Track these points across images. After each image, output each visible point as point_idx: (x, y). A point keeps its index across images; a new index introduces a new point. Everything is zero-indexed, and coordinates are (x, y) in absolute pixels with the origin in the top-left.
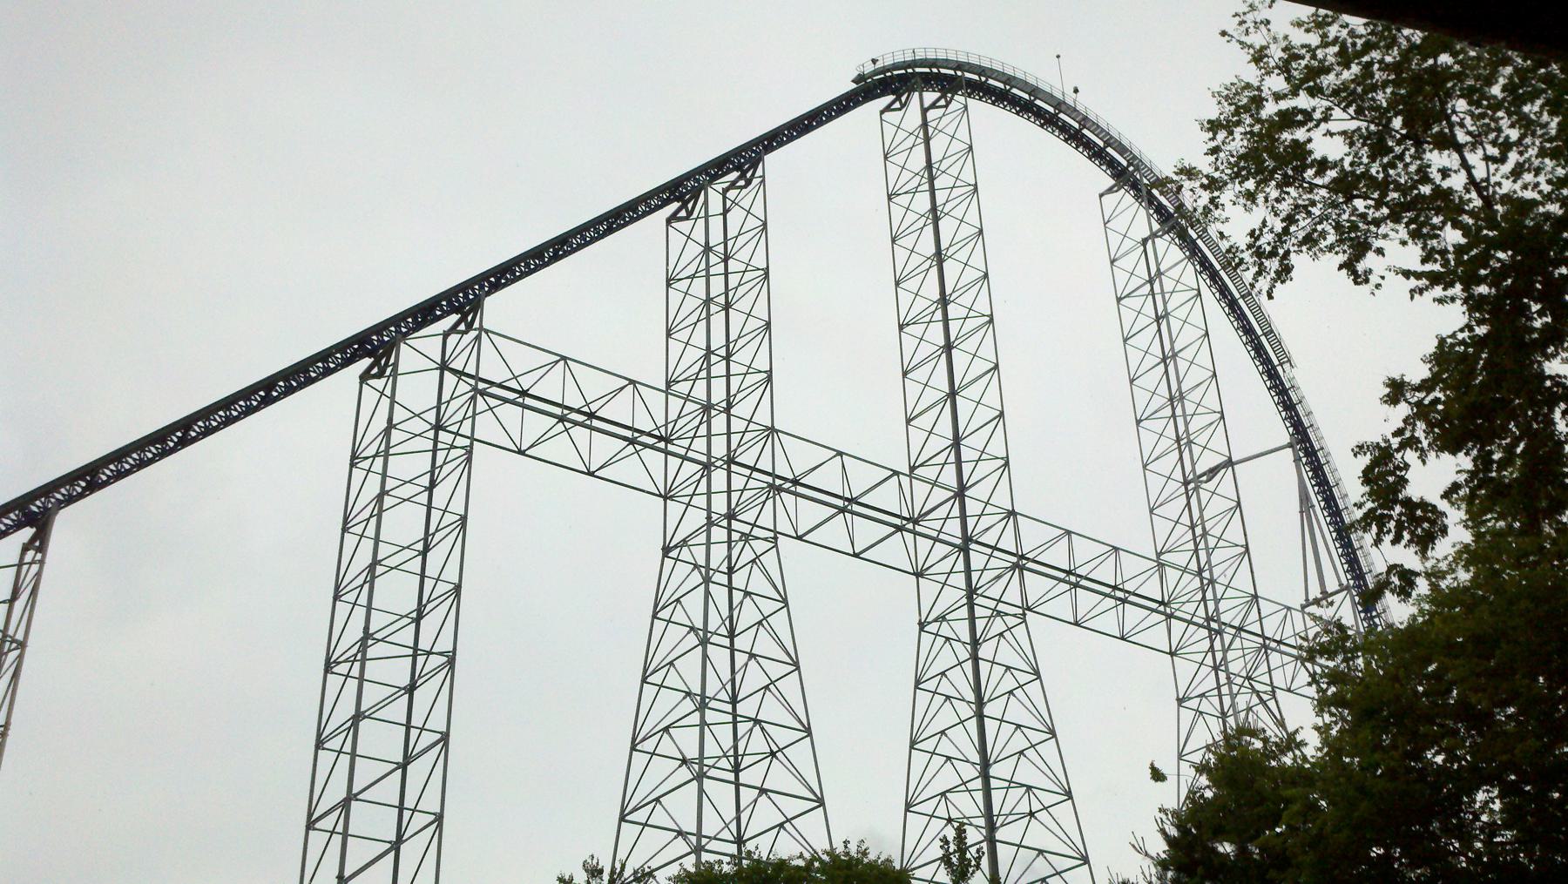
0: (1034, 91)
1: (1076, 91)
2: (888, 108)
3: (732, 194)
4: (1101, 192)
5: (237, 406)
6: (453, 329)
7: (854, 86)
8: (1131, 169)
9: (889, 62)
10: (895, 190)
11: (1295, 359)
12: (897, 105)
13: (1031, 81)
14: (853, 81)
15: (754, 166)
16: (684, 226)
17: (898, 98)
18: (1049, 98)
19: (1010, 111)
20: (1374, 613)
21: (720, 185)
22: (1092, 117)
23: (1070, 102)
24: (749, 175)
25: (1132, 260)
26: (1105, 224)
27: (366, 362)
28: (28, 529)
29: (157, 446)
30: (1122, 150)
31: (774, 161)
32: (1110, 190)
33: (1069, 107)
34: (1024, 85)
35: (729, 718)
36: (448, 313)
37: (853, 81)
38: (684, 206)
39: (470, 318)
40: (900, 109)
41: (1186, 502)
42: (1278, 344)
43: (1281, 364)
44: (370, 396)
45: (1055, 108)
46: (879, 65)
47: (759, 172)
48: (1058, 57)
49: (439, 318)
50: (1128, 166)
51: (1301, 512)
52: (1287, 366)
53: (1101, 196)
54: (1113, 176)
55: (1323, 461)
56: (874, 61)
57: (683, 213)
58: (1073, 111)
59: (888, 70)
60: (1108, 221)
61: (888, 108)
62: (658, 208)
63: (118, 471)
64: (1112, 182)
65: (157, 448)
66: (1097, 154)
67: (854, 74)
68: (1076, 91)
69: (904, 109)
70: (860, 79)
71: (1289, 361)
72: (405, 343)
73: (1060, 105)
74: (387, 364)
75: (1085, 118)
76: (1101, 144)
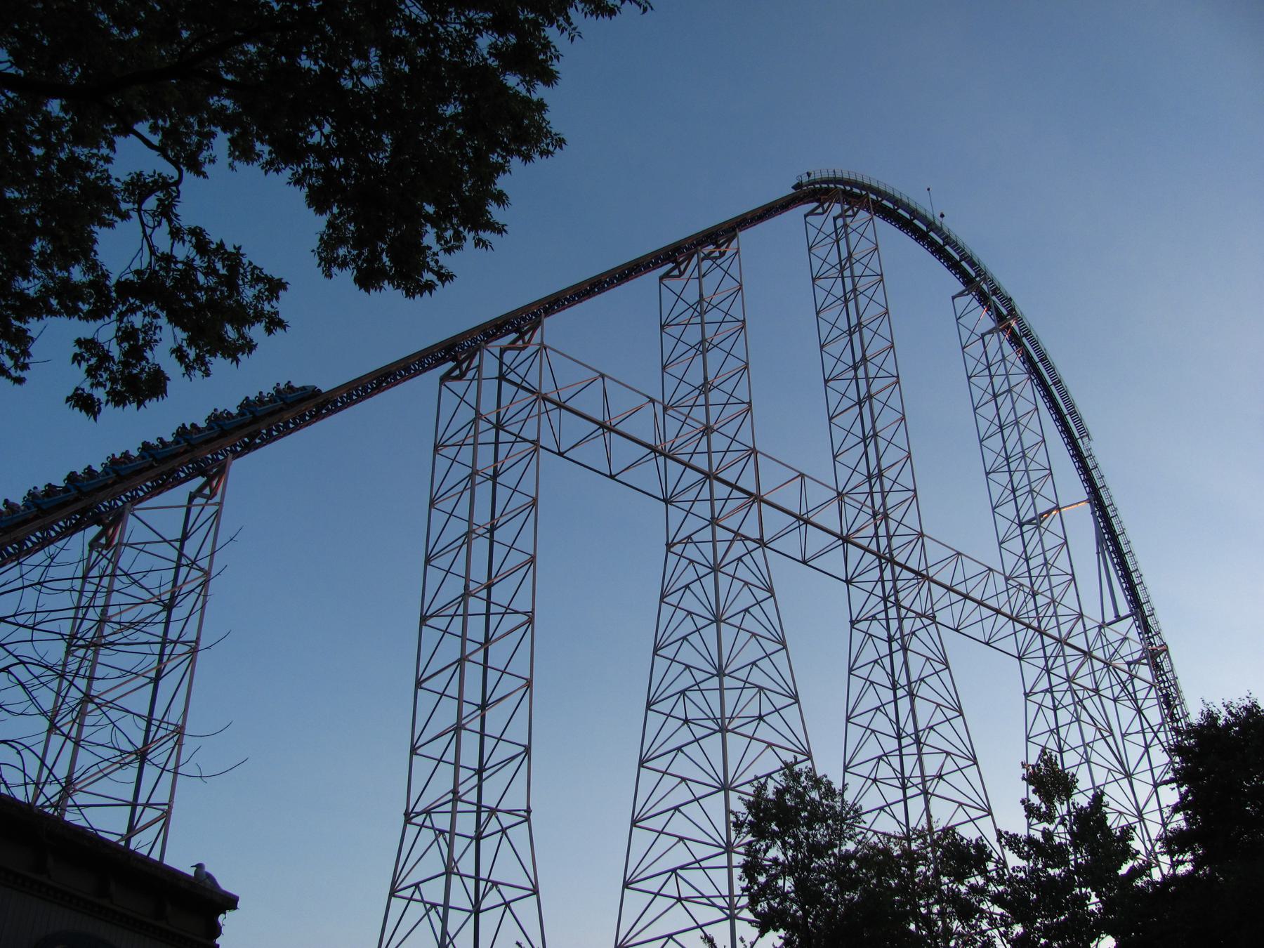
0: (914, 213)
1: (942, 216)
2: (812, 213)
3: (509, 357)
4: (954, 294)
5: (146, 490)
6: (199, 491)
7: (794, 191)
8: (978, 279)
9: (818, 177)
10: (442, 442)
11: (1092, 434)
12: (820, 210)
13: (912, 205)
14: (793, 188)
15: (471, 357)
16: (459, 386)
17: (821, 205)
18: (923, 219)
19: (895, 225)
20: (1150, 635)
21: (495, 346)
22: (953, 237)
23: (938, 223)
24: (464, 366)
25: (976, 349)
26: (957, 320)
27: (95, 530)
28: (200, 477)
29: (15, 545)
30: (972, 264)
31: (552, 324)
32: (961, 294)
33: (937, 227)
34: (907, 207)
35: (475, 808)
36: (511, 332)
37: (793, 188)
38: (458, 366)
39: (215, 483)
40: (822, 214)
41: (1039, 538)
42: (1079, 421)
43: (1081, 438)
44: (449, 401)
45: (927, 227)
46: (812, 177)
47: (475, 362)
48: (929, 189)
49: (506, 335)
50: (976, 277)
51: (1098, 553)
52: (1085, 439)
53: (953, 298)
54: (964, 283)
55: (1111, 514)
56: (809, 174)
57: (676, 272)
58: (939, 231)
59: (818, 183)
60: (960, 318)
61: (812, 213)
62: (431, 367)
63: (44, 538)
64: (963, 288)
65: (14, 548)
66: (954, 266)
67: (795, 182)
68: (942, 216)
69: (826, 215)
70: (798, 186)
71: (1088, 435)
72: (134, 515)
73: (931, 225)
74: (468, 368)
75: (948, 237)
76: (958, 258)
